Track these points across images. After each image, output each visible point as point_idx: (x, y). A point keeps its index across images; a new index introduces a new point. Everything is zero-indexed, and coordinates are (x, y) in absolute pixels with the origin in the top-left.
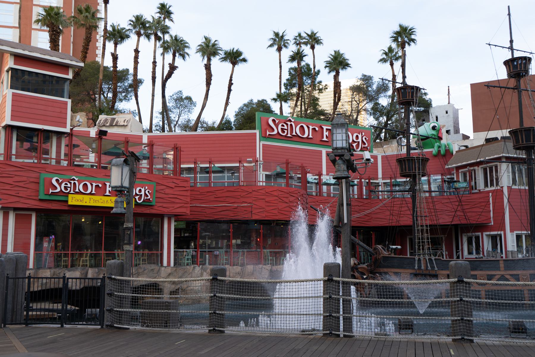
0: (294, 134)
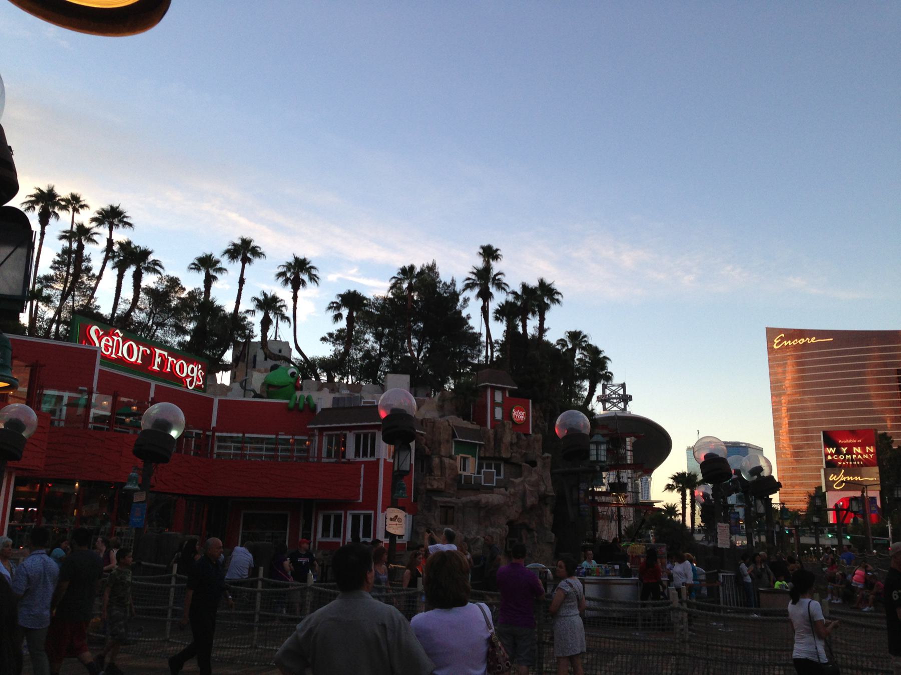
0: (120, 354)
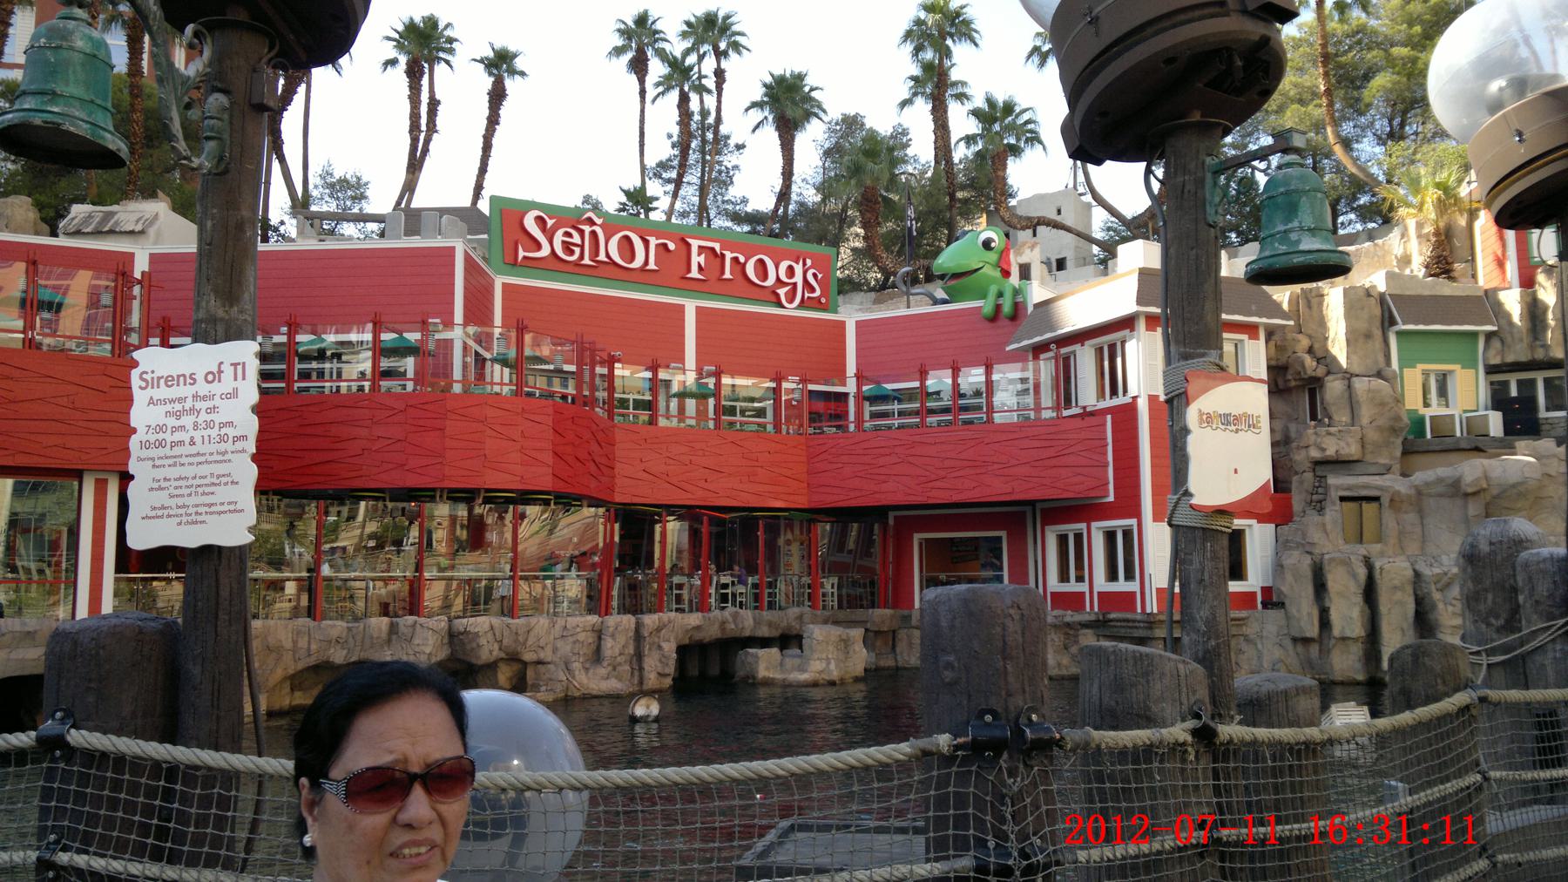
0: (602, 257)
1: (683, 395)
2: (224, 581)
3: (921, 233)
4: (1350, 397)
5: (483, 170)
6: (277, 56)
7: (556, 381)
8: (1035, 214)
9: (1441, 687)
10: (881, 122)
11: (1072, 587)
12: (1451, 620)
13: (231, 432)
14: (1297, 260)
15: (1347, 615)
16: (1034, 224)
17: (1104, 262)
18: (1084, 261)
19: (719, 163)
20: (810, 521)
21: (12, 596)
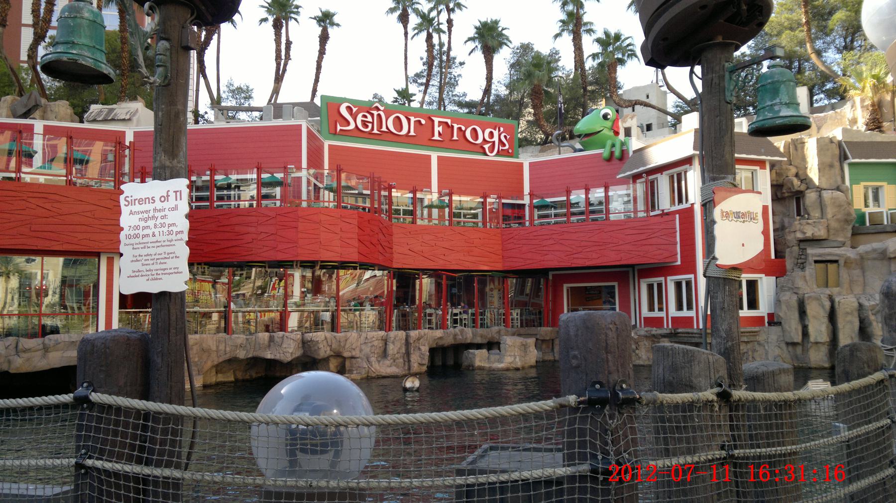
1: (430, 207)
2: (173, 311)
3: (567, 111)
4: (821, 202)
5: (317, 80)
6: (195, 19)
7: (360, 200)
8: (633, 98)
9: (866, 369)
10: (543, 47)
11: (656, 314)
12: (878, 329)
13: (175, 229)
14: (779, 122)
15: (819, 329)
16: (633, 104)
17: (674, 125)
18: (662, 125)
19: (450, 73)
20: (506, 277)
21: (64, 322)
